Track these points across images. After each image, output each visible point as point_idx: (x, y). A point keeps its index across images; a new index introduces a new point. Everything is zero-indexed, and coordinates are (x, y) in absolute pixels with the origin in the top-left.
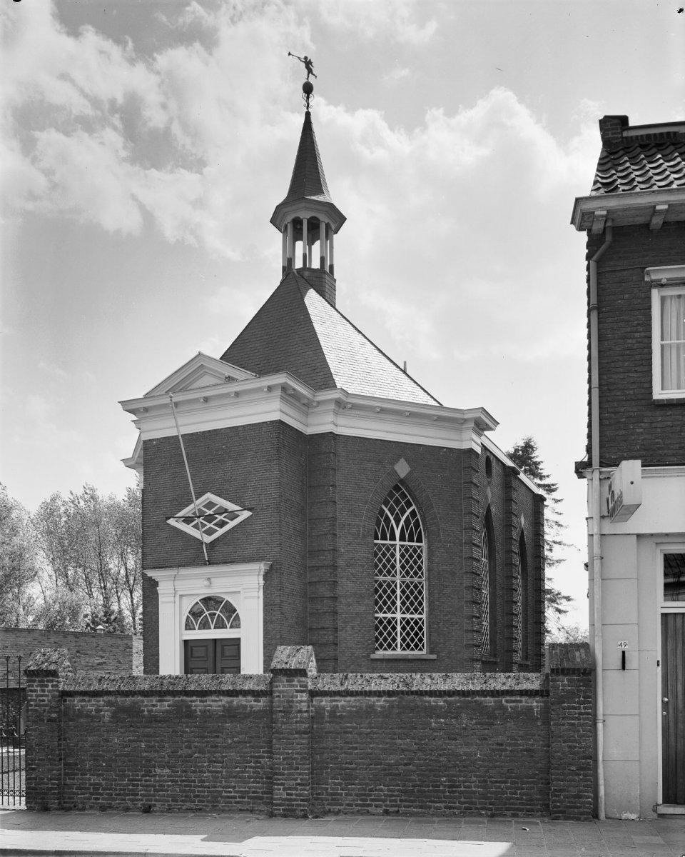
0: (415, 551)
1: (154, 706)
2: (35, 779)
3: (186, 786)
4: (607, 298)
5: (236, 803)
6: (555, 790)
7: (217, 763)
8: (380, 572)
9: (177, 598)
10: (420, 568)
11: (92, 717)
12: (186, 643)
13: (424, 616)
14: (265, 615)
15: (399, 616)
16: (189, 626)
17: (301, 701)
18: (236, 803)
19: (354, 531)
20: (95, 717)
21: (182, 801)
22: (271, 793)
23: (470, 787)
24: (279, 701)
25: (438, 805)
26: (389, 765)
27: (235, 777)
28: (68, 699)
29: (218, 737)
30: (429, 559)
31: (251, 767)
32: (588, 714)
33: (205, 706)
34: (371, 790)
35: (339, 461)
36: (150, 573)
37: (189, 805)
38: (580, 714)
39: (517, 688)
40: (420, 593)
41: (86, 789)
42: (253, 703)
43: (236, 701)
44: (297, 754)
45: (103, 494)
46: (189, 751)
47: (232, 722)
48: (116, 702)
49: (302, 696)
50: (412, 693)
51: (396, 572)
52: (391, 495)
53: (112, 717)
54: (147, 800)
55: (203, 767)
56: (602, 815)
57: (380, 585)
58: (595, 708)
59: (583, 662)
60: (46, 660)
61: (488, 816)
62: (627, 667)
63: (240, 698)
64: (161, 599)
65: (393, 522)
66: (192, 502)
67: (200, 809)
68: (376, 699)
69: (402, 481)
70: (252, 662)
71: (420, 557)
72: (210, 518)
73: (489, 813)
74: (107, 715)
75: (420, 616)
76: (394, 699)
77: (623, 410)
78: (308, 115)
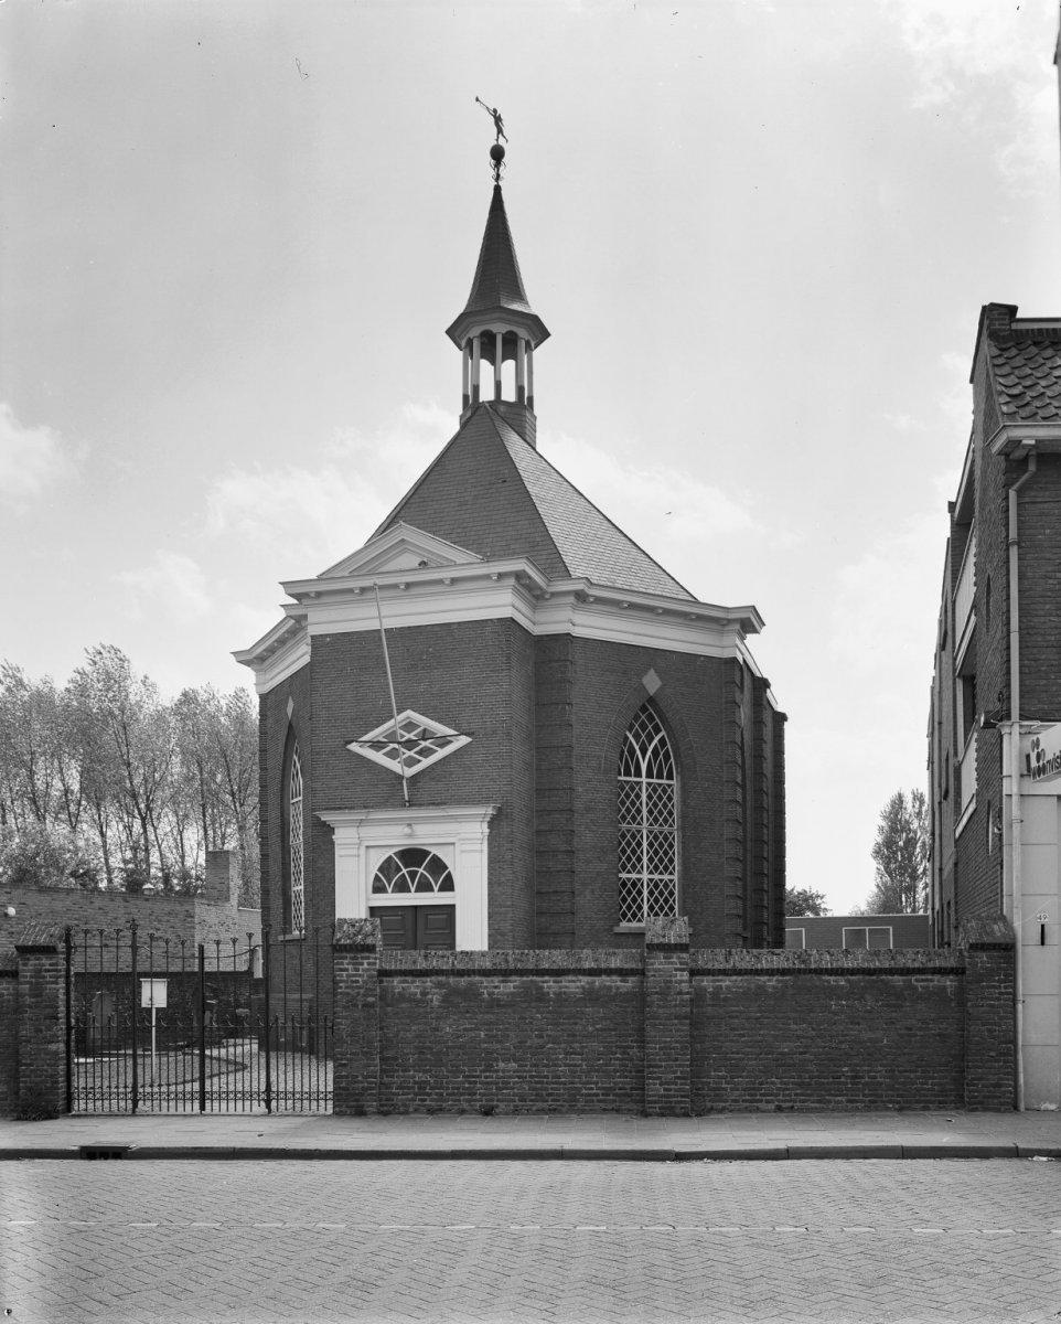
0: (665, 791)
1: (496, 987)
2: (347, 1077)
3: (536, 1083)
4: (1027, 532)
5: (599, 1101)
6: (973, 1079)
7: (576, 1054)
8: (624, 818)
9: (363, 849)
10: (670, 813)
11: (419, 1001)
13: (675, 877)
14: (490, 874)
15: (645, 876)
16: (378, 888)
17: (682, 981)
18: (599, 1101)
19: (594, 763)
20: (421, 1001)
21: (531, 1101)
22: (643, 1089)
23: (875, 1077)
24: (654, 981)
25: (840, 1098)
26: (782, 1054)
27: (597, 1071)
28: (385, 979)
29: (576, 1024)
30: (684, 802)
31: (617, 1059)
32: (1007, 993)
33: (561, 988)
34: (761, 1084)
35: (575, 672)
36: (326, 817)
37: (540, 1105)
38: (1001, 993)
39: (931, 965)
40: (671, 846)
41: (409, 1088)
42: (619, 983)
43: (598, 981)
44: (677, 1042)
45: (33, 678)
46: (541, 1041)
47: (593, 1007)
48: (448, 983)
49: (681, 976)
50: (811, 971)
51: (642, 818)
52: (637, 717)
53: (443, 1001)
54: (487, 1100)
55: (557, 1059)
56: (1022, 1106)
57: (624, 836)
58: (1015, 987)
59: (1004, 935)
60: (359, 933)
61: (895, 1109)
62: (1046, 941)
63: (604, 977)
64: (338, 852)
65: (638, 752)
66: (392, 717)
67: (555, 1110)
68: (766, 978)
69: (651, 700)
70: (472, 934)
71: (670, 799)
72: (410, 744)
73: (897, 1106)
74: (436, 1000)
75: (671, 877)
76: (788, 978)
77: (1043, 657)
78: (497, 189)
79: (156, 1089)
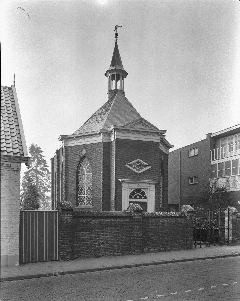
12: (130, 202)
16: (130, 197)
70: (151, 209)
72: (138, 166)
78: (116, 43)
79: (185, 236)
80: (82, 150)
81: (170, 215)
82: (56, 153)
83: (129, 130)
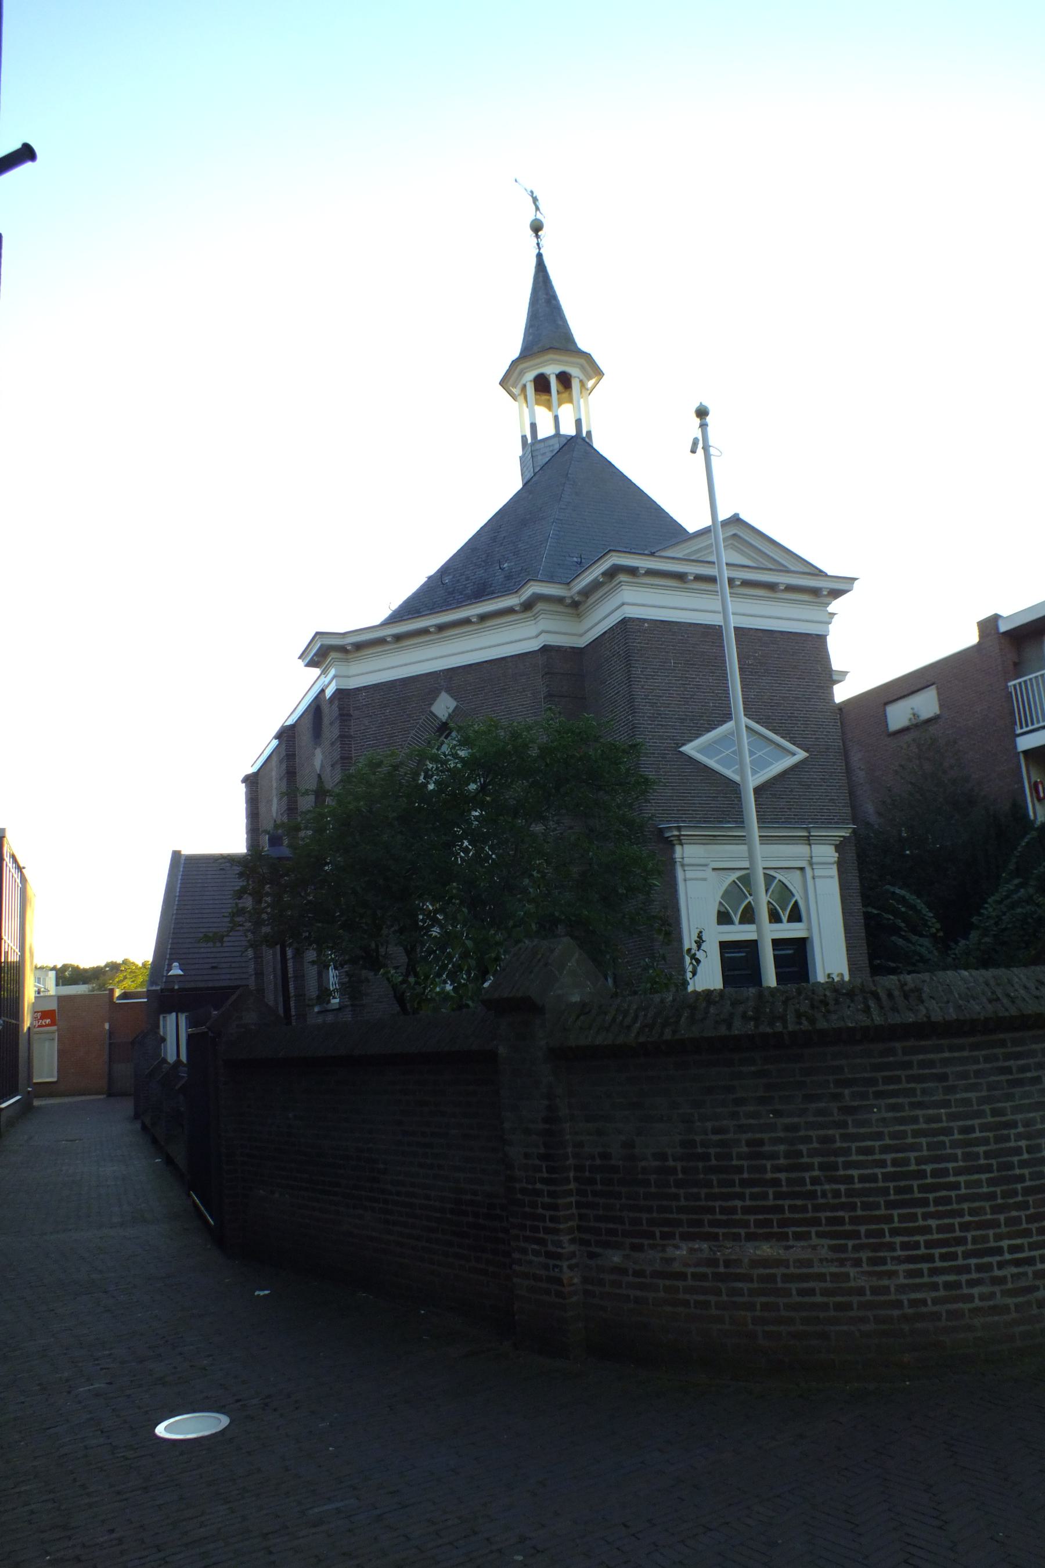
16: (724, 918)
78: (539, 256)
80: (432, 695)
81: (979, 1009)
82: (275, 742)
83: (680, 577)
